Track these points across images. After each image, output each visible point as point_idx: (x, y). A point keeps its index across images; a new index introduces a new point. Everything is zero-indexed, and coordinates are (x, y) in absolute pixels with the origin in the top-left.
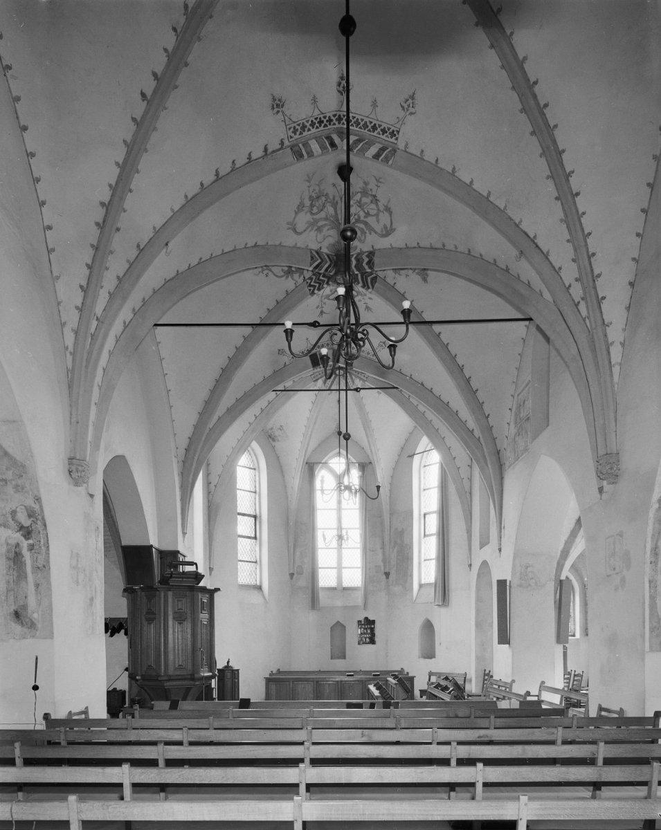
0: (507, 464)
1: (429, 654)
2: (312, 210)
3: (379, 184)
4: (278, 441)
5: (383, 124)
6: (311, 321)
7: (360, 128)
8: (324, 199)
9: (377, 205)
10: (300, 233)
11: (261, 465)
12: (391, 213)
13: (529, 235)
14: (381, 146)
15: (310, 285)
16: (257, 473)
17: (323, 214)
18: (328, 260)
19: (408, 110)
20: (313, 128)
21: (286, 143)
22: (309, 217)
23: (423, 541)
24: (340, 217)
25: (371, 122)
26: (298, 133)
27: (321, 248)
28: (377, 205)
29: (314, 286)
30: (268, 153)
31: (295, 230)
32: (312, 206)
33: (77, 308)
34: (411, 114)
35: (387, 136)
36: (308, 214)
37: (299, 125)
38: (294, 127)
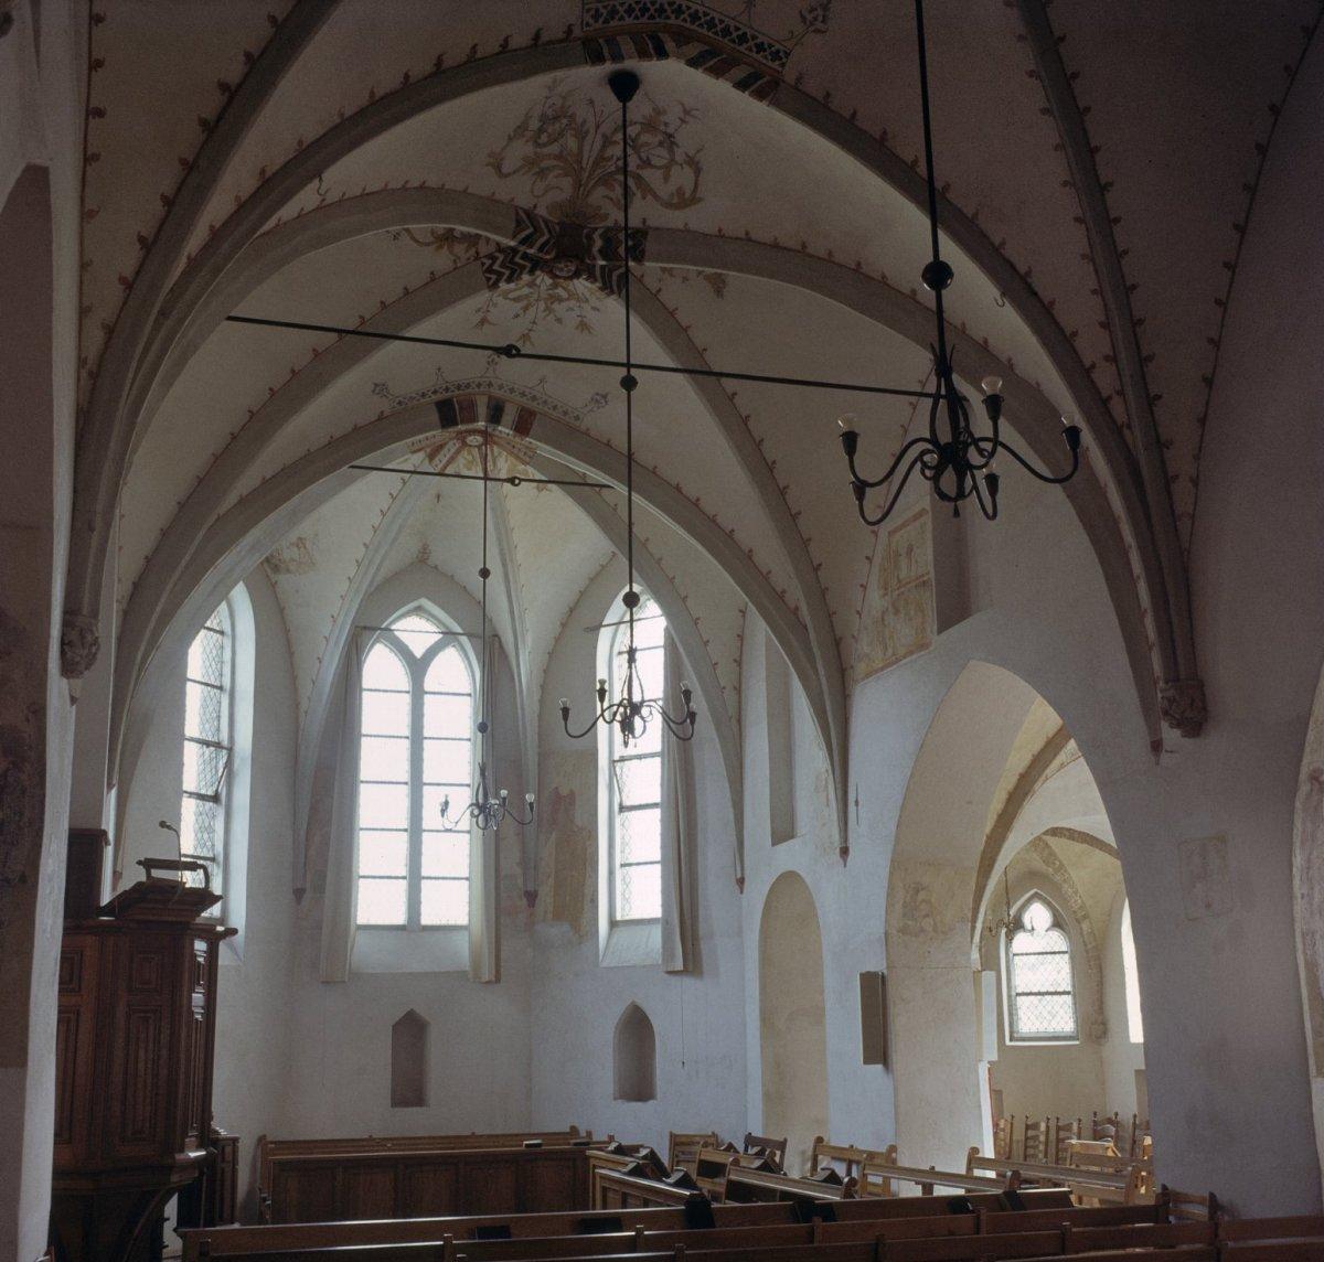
0: (861, 668)
1: (638, 1085)
2: (539, 137)
3: (688, 118)
4: (288, 571)
5: (760, 36)
6: (503, 344)
7: (716, 33)
8: (565, 121)
9: (671, 151)
10: (506, 176)
11: (240, 628)
12: (698, 171)
13: (1018, 267)
14: (752, 71)
15: (490, 270)
16: (227, 642)
17: (554, 149)
18: (546, 230)
19: (812, 24)
20: (630, 16)
21: (577, 32)
22: (529, 149)
23: (618, 819)
24: (585, 162)
25: (738, 29)
26: (601, 20)
27: (535, 206)
28: (671, 151)
29: (500, 275)
30: (540, 42)
31: (498, 168)
32: (541, 130)
33: (122, 280)
34: (818, 31)
35: (766, 58)
36: (530, 144)
37: (605, 7)
38: (597, 10)
